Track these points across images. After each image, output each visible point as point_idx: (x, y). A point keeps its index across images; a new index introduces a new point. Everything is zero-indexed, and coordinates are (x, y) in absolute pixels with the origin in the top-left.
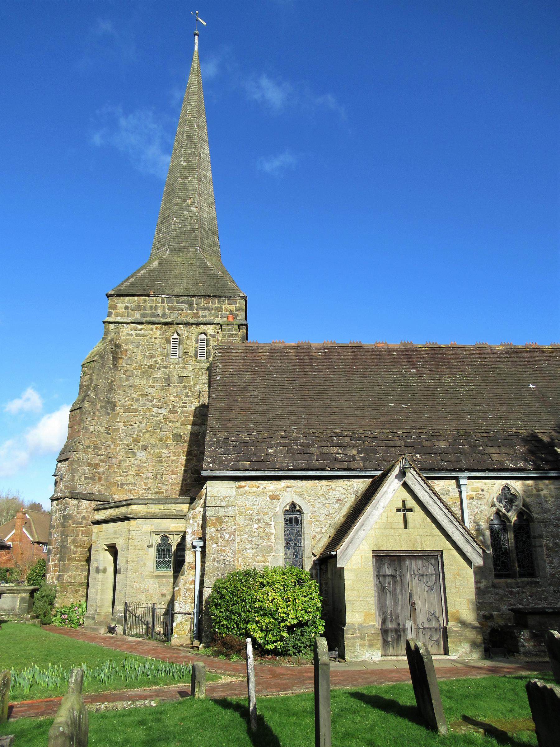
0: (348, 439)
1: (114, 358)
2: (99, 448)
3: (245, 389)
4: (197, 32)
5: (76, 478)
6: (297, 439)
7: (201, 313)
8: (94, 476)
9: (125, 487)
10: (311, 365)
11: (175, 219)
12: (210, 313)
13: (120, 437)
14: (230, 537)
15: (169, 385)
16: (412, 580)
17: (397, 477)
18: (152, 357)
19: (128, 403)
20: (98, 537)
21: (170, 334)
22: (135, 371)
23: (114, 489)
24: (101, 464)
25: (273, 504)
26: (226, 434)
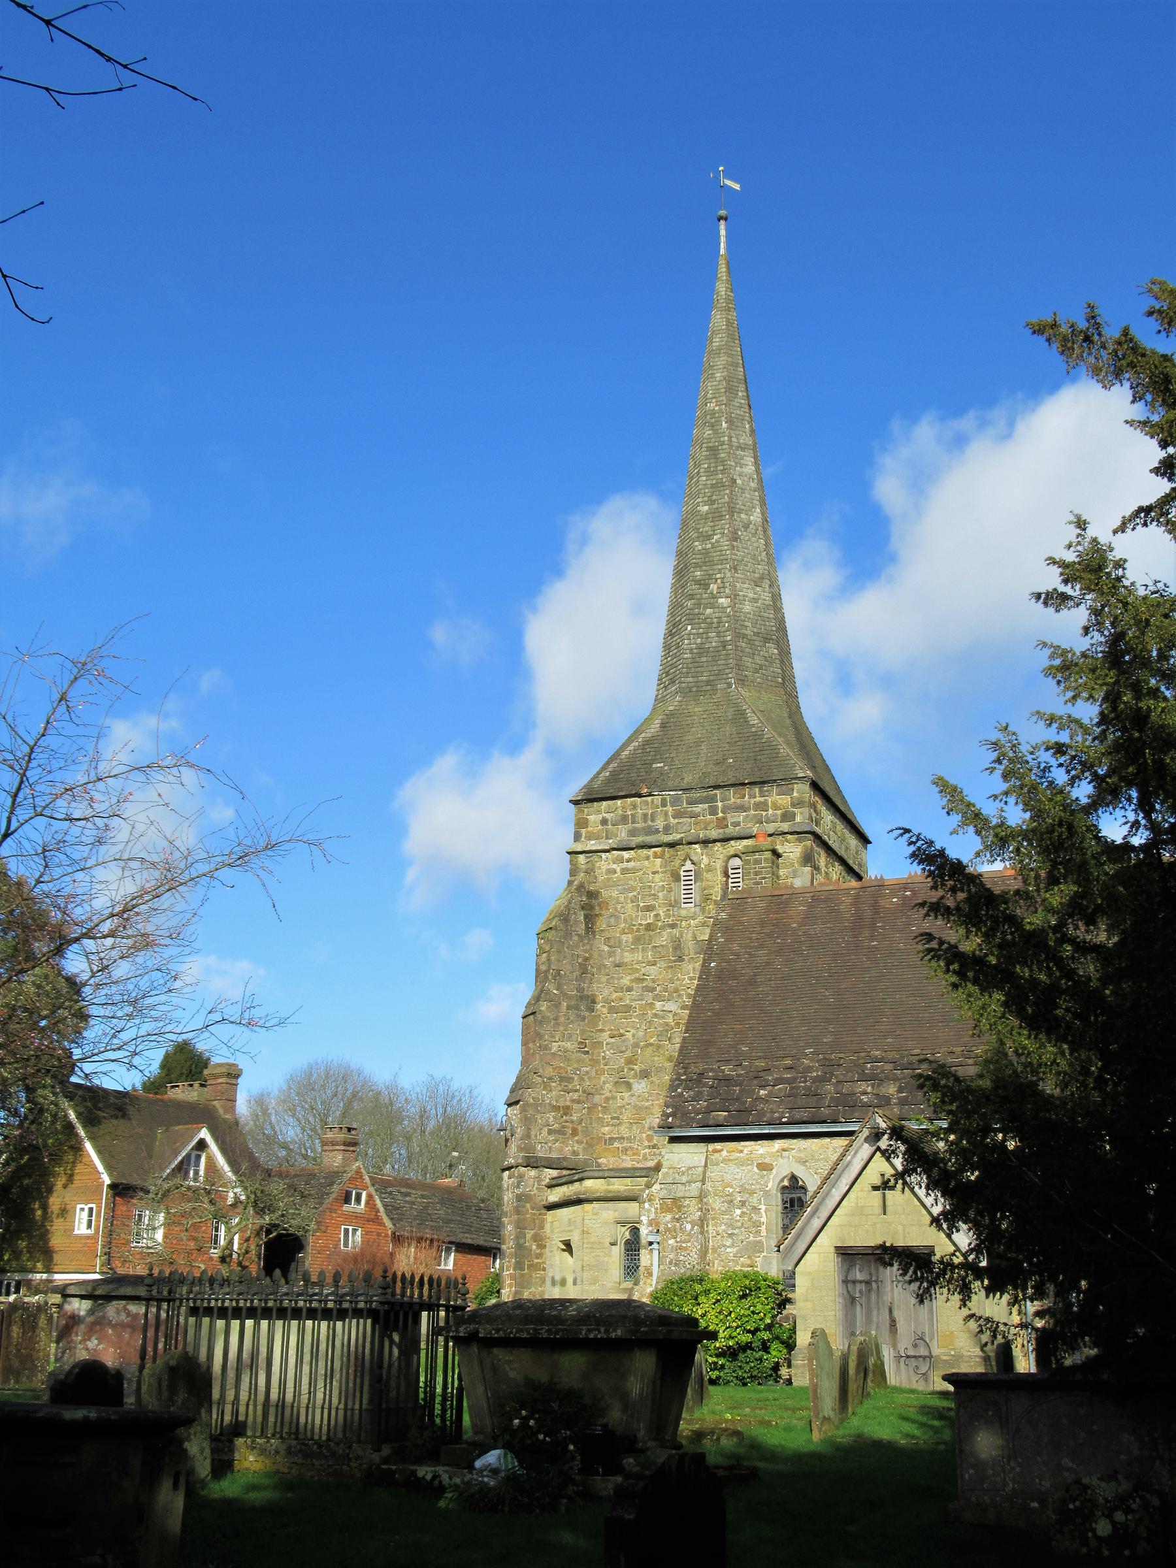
0: (889, 1067)
1: (586, 917)
2: (570, 1080)
3: (752, 982)
4: (722, 213)
5: (533, 1133)
6: (809, 1069)
7: (731, 818)
8: (564, 1127)
9: (616, 1144)
10: (873, 926)
11: (689, 628)
12: (747, 816)
13: (604, 1058)
14: (693, 1228)
15: (681, 959)
16: (892, 1289)
17: (866, 1140)
18: (649, 908)
19: (615, 995)
20: (552, 1231)
21: (677, 862)
22: (624, 938)
23: (600, 1148)
24: (575, 1106)
25: (763, 1177)
26: (702, 1067)
